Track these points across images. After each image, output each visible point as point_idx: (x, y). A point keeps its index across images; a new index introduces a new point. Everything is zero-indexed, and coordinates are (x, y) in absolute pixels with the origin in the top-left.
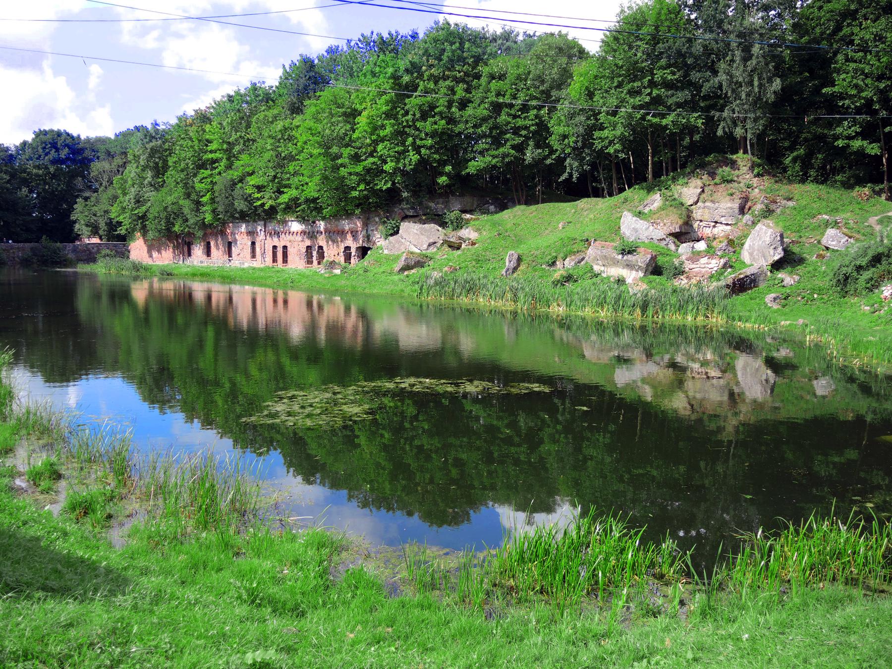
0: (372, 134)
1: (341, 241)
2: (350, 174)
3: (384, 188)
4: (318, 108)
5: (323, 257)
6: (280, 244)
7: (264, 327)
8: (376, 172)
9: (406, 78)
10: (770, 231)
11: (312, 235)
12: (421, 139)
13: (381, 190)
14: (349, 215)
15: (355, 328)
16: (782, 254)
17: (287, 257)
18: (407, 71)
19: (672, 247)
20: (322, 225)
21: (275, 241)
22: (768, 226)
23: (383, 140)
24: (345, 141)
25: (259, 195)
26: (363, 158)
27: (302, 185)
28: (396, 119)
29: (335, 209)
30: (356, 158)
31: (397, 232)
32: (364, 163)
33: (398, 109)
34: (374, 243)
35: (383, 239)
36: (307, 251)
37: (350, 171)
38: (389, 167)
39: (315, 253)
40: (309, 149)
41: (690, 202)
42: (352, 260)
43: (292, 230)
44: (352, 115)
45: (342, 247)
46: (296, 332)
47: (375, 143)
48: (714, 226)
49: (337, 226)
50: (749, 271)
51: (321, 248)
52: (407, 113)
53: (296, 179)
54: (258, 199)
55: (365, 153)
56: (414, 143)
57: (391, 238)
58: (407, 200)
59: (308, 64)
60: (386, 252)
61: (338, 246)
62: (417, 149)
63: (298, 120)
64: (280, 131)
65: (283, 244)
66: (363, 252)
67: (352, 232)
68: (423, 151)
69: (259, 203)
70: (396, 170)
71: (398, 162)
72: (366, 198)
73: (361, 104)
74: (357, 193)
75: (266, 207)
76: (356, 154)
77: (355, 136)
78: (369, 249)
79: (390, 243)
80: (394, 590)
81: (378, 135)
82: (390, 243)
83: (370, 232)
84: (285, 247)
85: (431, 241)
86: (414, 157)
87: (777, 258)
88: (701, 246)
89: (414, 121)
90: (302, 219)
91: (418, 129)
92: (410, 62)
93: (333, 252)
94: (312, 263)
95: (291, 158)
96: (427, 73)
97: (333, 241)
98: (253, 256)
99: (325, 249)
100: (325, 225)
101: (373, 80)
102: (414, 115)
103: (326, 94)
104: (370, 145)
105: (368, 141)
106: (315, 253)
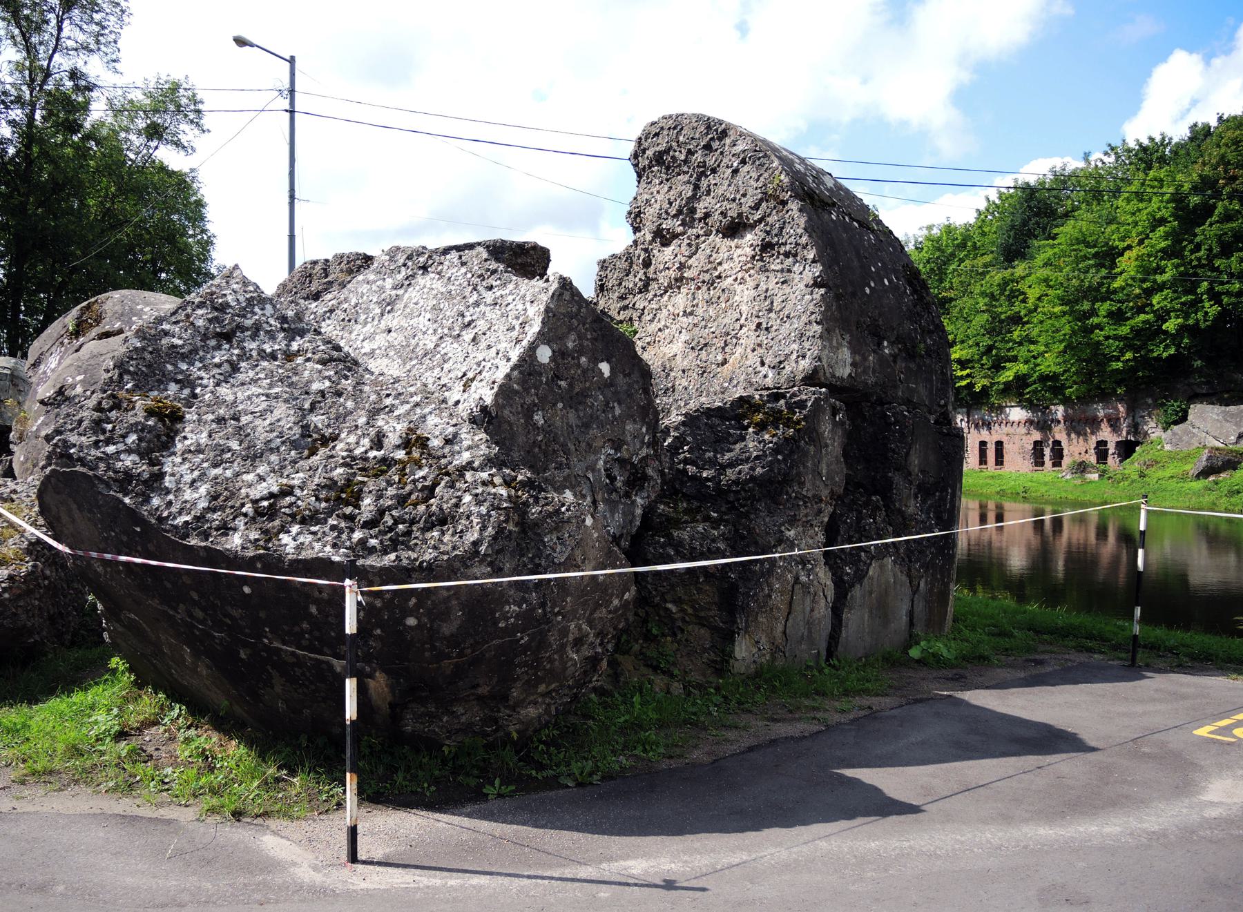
0: (1143, 281)
1: (1092, 433)
2: (1107, 338)
3: (1165, 355)
4: (1056, 250)
5: (1062, 457)
6: (990, 437)
7: (965, 552)
8: (1151, 333)
9: (1195, 200)
11: (1044, 426)
12: (1222, 283)
13: (1159, 358)
14: (1105, 397)
15: (1116, 560)
17: (1002, 456)
18: (1195, 189)
20: (1059, 411)
21: (984, 435)
23: (1161, 287)
24: (1096, 293)
25: (964, 373)
26: (1129, 314)
27: (1035, 357)
28: (1182, 257)
29: (1084, 388)
30: (1118, 317)
31: (1184, 419)
32: (1132, 322)
33: (1185, 243)
34: (1146, 434)
35: (1160, 429)
36: (1034, 448)
37: (1106, 334)
38: (1170, 325)
39: (1047, 451)
40: (1045, 307)
42: (1110, 460)
43: (1011, 418)
44: (1109, 257)
45: (1093, 440)
46: (1017, 561)
47: (1149, 293)
49: (1084, 412)
51: (1057, 443)
52: (1198, 248)
53: (1023, 349)
54: (962, 378)
55: (1132, 308)
56: (1210, 291)
57: (1175, 428)
58: (1199, 371)
59: (1029, 192)
60: (1168, 447)
61: (1086, 440)
62: (1215, 297)
63: (1020, 269)
64: (999, 285)
65: (996, 438)
66: (1126, 449)
67: (1109, 421)
68: (1225, 300)
69: (964, 383)
70: (1182, 329)
71: (1186, 317)
72: (1133, 370)
73: (1122, 239)
74: (1120, 364)
75: (977, 389)
76: (1119, 309)
77: (1116, 285)
78: (1138, 443)
79: (1174, 434)
81: (1155, 281)
82: (1174, 434)
83: (1139, 420)
84: (999, 444)
86: (1212, 310)
89: (1210, 258)
90: (1029, 405)
91: (1217, 269)
92: (1200, 176)
93: (1077, 449)
94: (1042, 464)
95: (1017, 320)
96: (1228, 189)
97: (1079, 434)
99: (1064, 444)
100: (1066, 411)
101: (1141, 205)
102: (1210, 249)
103: (1067, 230)
104: (1138, 296)
105: (1137, 291)
106: (1047, 451)
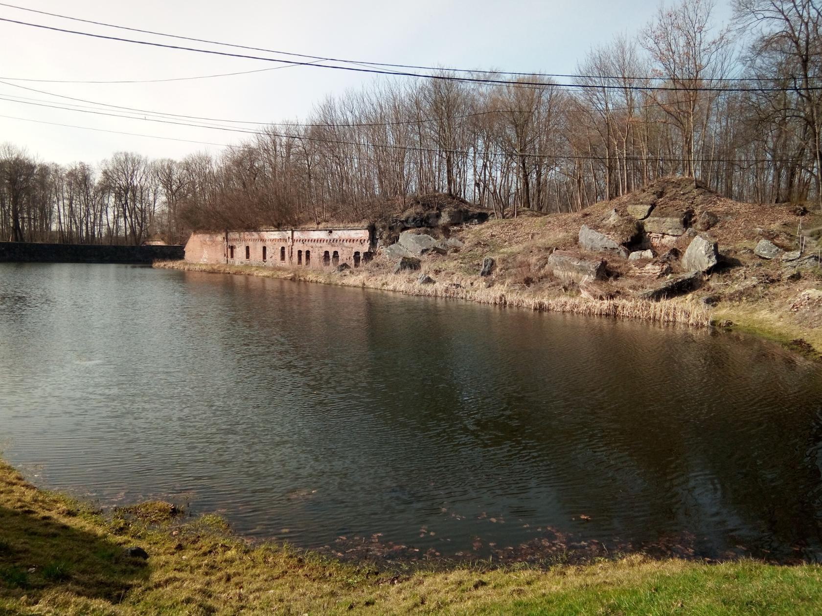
10: (705, 242)
16: (715, 262)
19: (623, 254)
22: (705, 238)
41: (642, 216)
48: (663, 237)
50: (688, 276)
65: (306, 249)
80: (565, 583)
84: (308, 252)
85: (424, 248)
87: (711, 265)
88: (648, 254)
98: (283, 258)
